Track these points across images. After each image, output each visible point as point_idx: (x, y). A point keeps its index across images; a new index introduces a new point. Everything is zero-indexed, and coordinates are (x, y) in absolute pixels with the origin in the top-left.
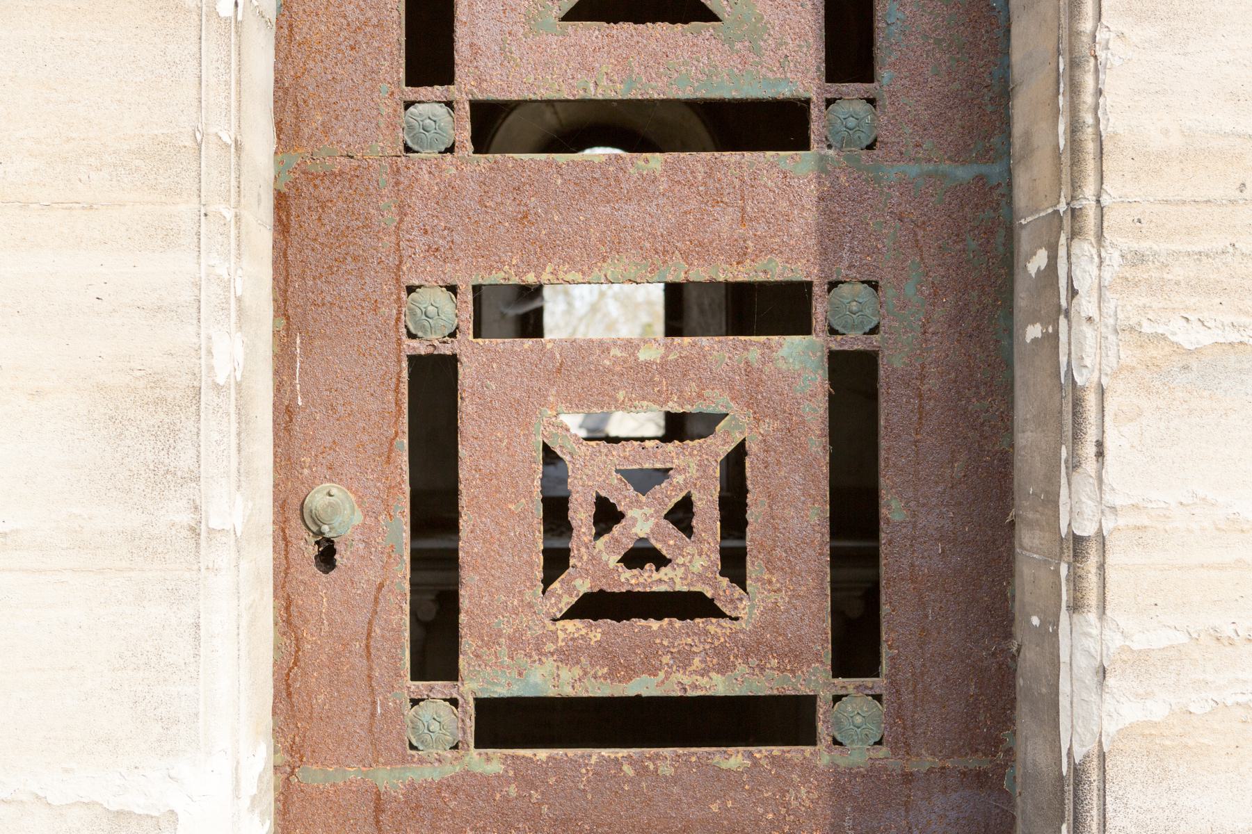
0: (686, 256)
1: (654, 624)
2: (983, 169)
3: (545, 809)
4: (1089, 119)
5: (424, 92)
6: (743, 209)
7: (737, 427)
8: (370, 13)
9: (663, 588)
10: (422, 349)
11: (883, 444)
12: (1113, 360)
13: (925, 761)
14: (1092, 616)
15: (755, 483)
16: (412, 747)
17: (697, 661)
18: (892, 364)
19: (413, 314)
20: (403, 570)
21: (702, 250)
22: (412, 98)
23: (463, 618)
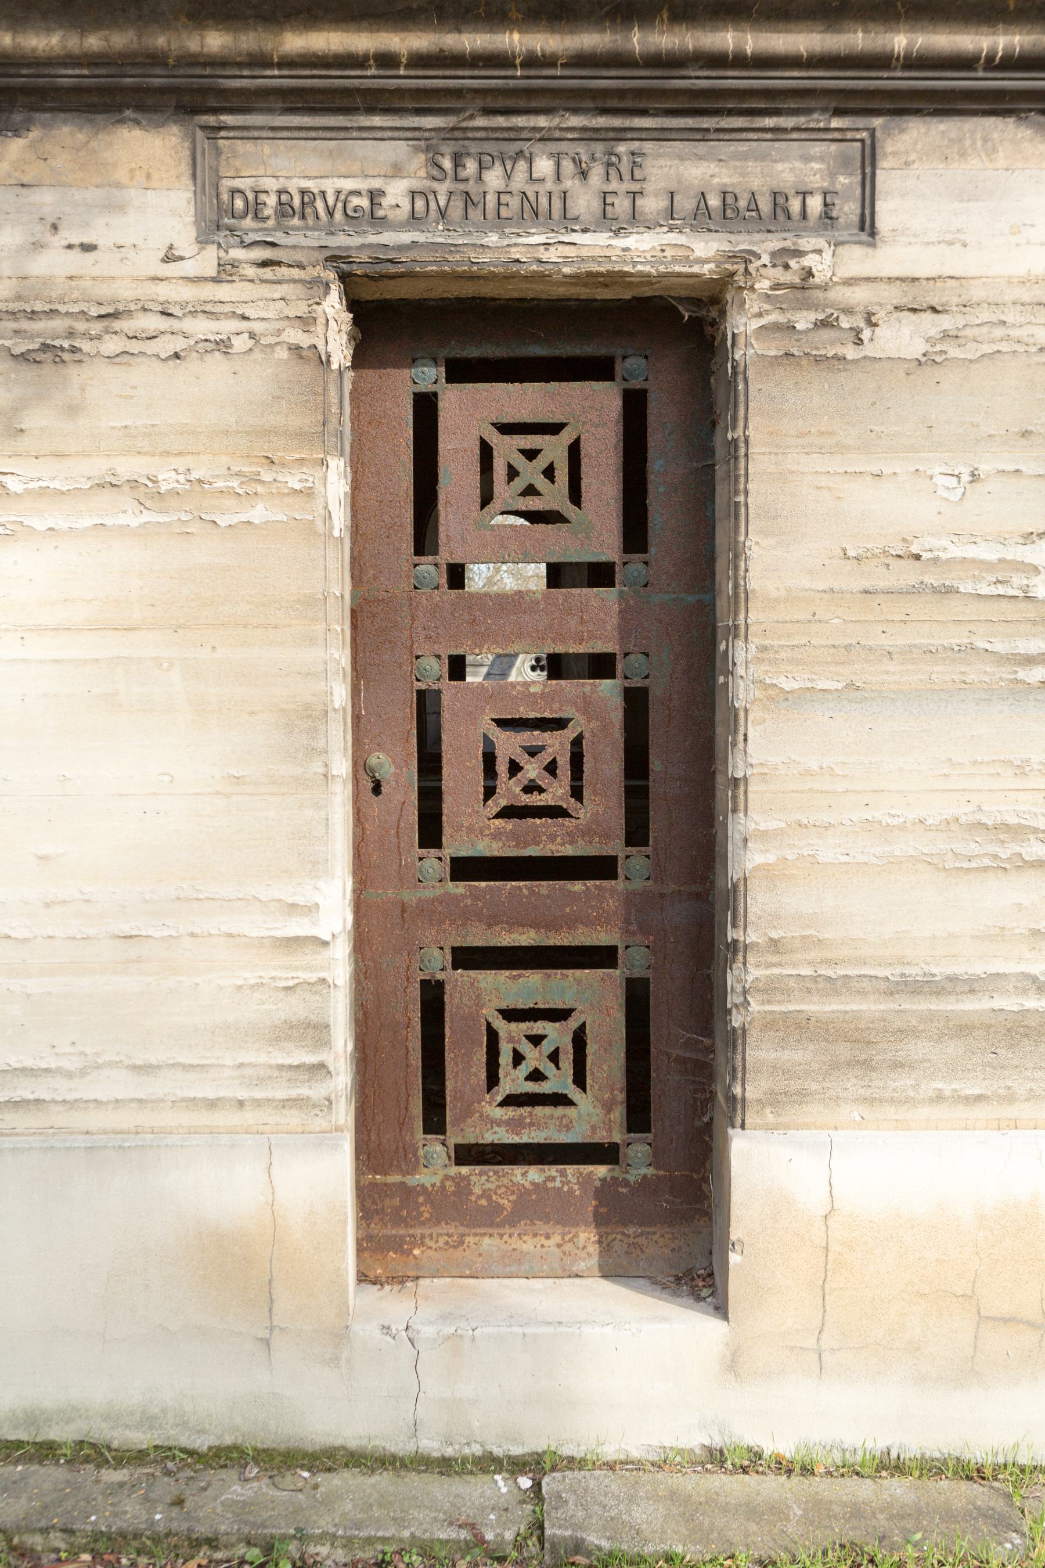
0: (554, 641)
1: (538, 821)
2: (701, 597)
3: (485, 910)
4: (742, 583)
5: (423, 559)
6: (582, 617)
7: (579, 724)
8: (396, 520)
9: (542, 803)
10: (422, 686)
11: (651, 733)
12: (752, 695)
13: (671, 887)
14: (741, 815)
15: (588, 752)
16: (420, 881)
17: (559, 839)
18: (656, 693)
19: (419, 669)
20: (414, 797)
21: (561, 637)
22: (417, 562)
23: (444, 818)
